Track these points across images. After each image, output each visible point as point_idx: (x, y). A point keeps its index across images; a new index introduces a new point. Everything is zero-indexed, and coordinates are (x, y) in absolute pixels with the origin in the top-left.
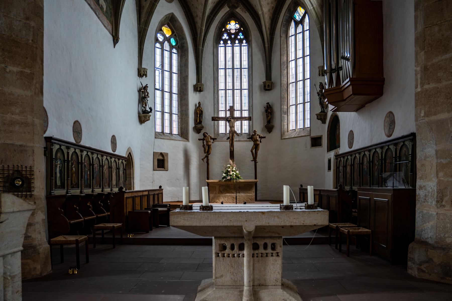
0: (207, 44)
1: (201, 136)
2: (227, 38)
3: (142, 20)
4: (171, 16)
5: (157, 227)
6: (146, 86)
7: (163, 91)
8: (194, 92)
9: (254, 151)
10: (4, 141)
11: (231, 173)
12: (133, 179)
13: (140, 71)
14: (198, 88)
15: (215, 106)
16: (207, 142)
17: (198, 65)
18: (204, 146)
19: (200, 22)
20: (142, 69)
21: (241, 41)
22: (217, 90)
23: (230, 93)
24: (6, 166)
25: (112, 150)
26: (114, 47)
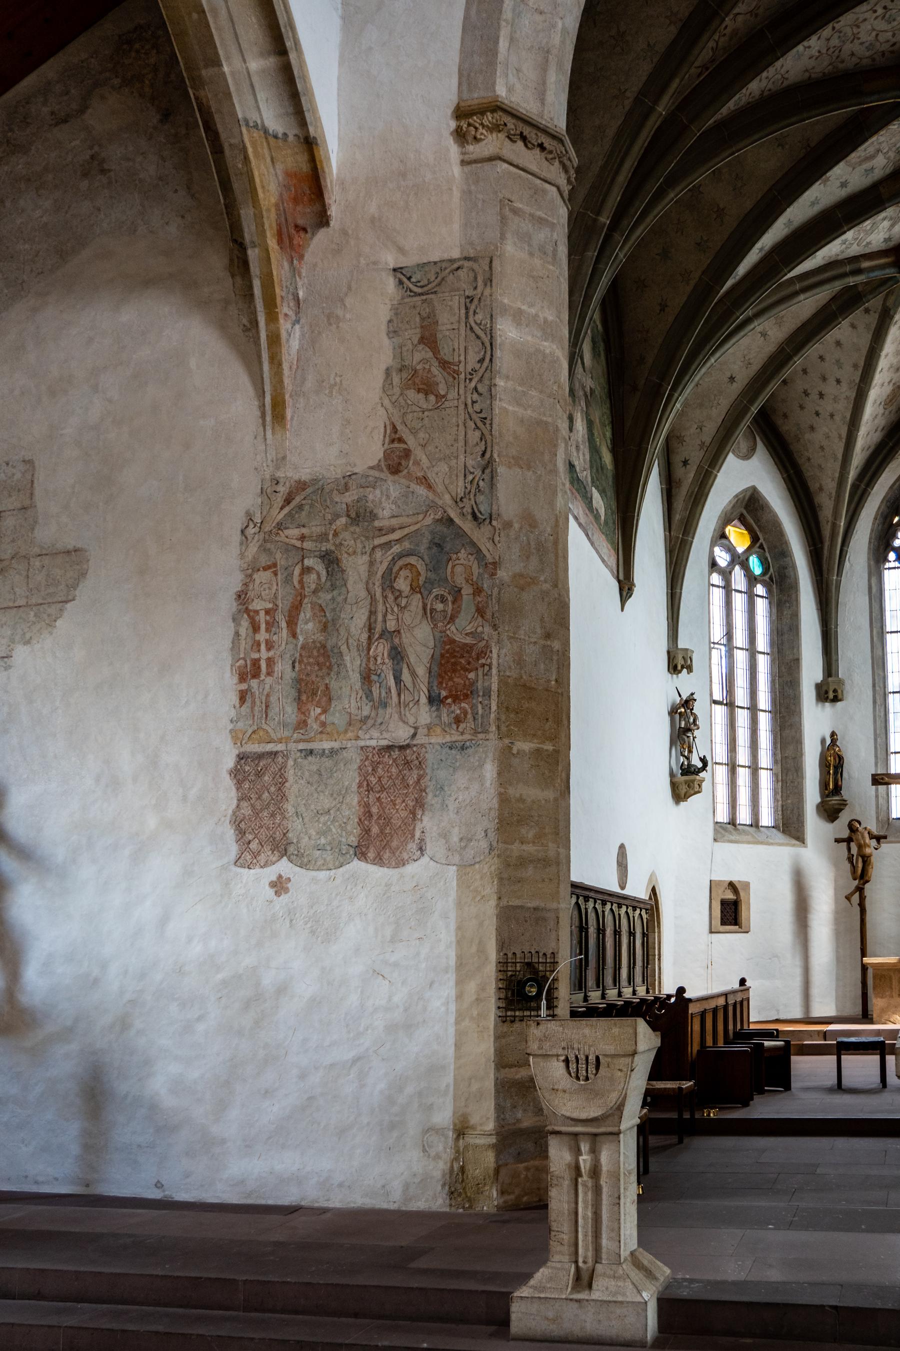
0: (852, 565)
1: (840, 828)
3: (677, 517)
4: (748, 494)
5: (762, 1092)
6: (691, 698)
7: (730, 705)
8: (817, 704)
10: (508, 902)
12: (659, 959)
13: (674, 657)
15: (879, 740)
16: (860, 847)
17: (827, 627)
18: (850, 859)
19: (831, 507)
20: (679, 652)
22: (882, 693)
24: (510, 955)
25: (620, 886)
26: (622, 610)
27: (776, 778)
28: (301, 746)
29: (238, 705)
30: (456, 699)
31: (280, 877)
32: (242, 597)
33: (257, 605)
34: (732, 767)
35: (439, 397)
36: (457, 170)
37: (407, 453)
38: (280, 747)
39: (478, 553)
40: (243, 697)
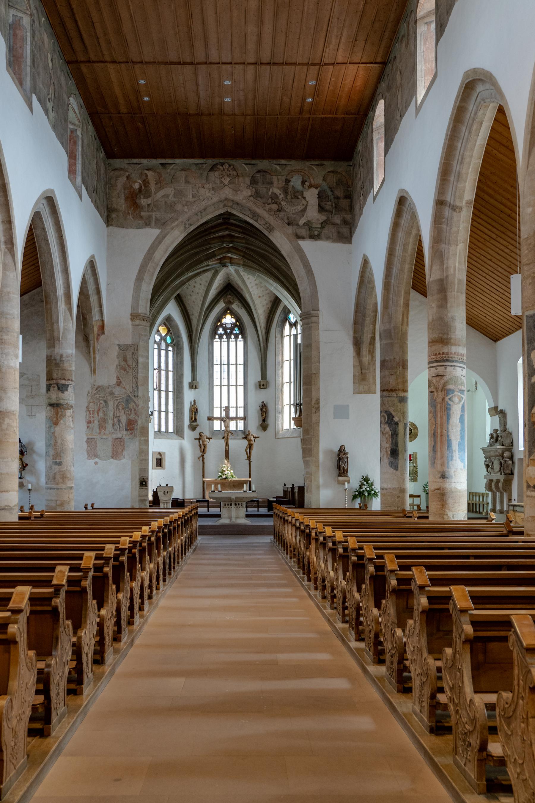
1: (196, 434)
2: (223, 332)
9: (248, 450)
11: (226, 472)
14: (193, 386)
16: (203, 441)
18: (200, 445)
21: (236, 337)
23: (225, 367)
27: (174, 415)
30: (131, 430)
32: (87, 407)
33: (90, 409)
34: (160, 412)
35: (127, 372)
36: (131, 326)
37: (121, 382)
39: (135, 403)
40: (88, 427)
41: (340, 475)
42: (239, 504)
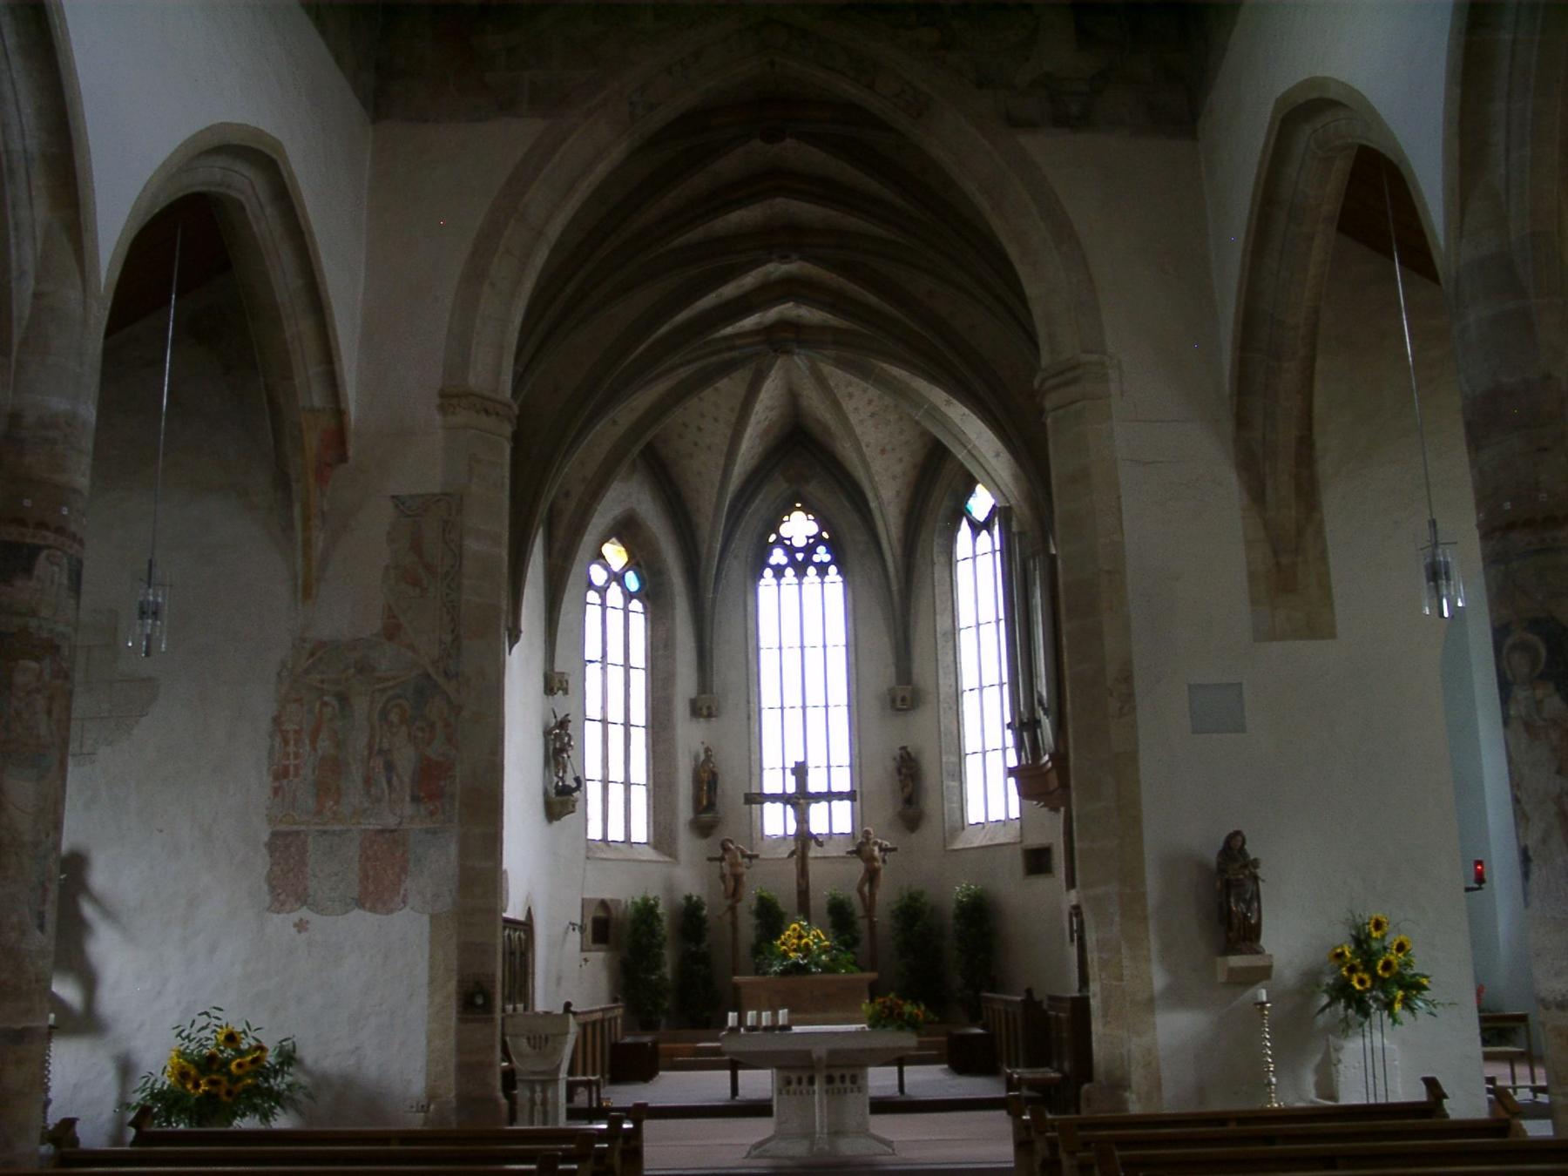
9: (866, 889)
14: (702, 709)
18: (723, 877)
21: (822, 569)
28: (320, 828)
29: (272, 797)
31: (301, 920)
32: (276, 720)
34: (605, 783)
38: (303, 828)
40: (276, 791)
41: (1230, 948)
42: (843, 1078)
